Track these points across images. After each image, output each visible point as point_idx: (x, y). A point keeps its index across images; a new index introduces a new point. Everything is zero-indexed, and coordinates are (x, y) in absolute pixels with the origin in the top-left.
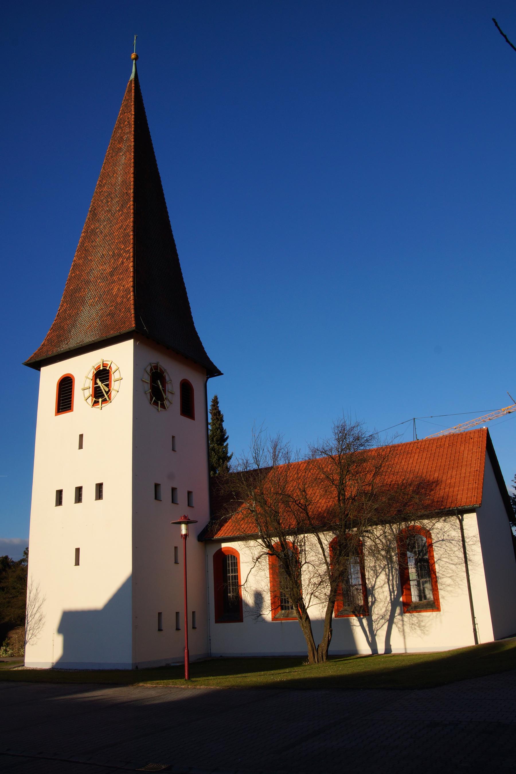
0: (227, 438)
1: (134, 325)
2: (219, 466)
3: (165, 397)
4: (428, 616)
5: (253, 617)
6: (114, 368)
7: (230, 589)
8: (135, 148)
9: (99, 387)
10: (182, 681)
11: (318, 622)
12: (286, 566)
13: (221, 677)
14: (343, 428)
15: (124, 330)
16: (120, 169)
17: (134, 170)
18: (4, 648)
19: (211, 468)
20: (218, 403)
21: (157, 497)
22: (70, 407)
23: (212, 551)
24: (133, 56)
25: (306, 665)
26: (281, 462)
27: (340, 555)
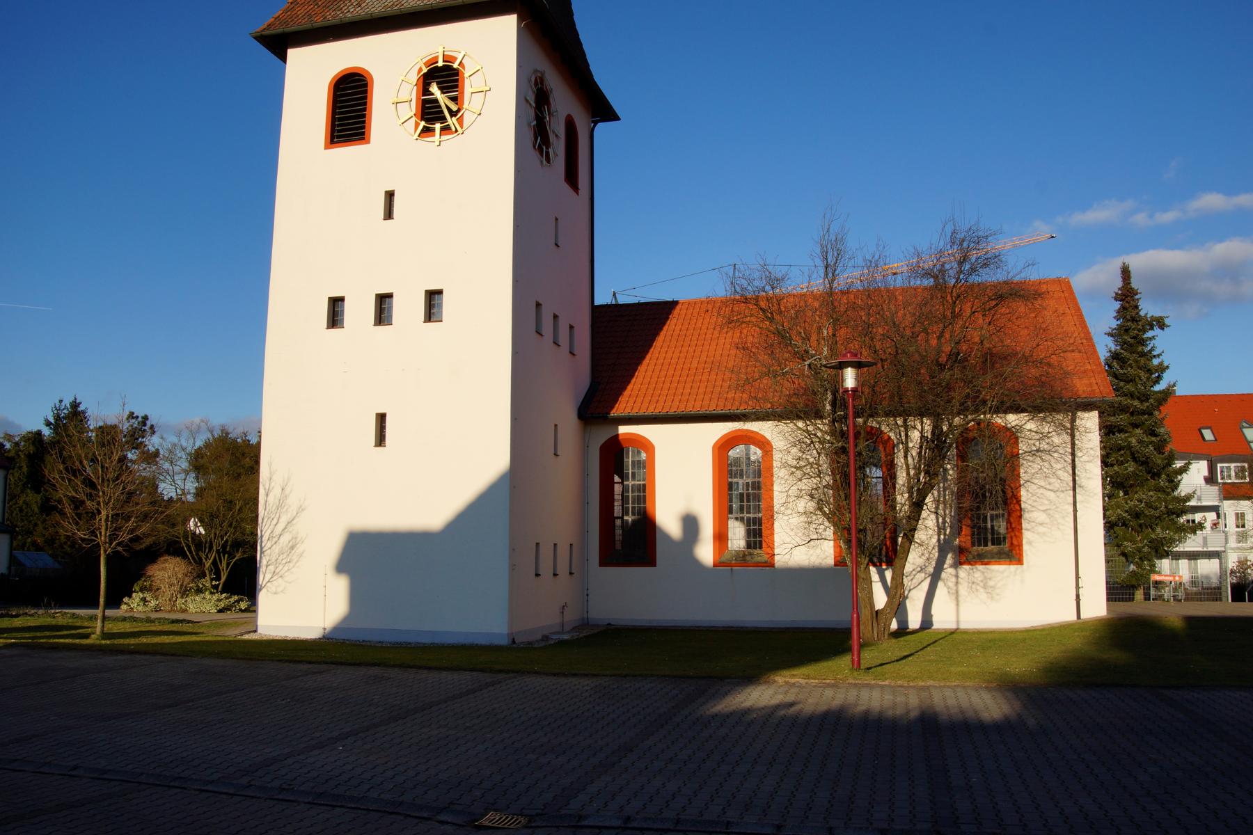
4: (1000, 572)
21: (433, 298)
22: (363, 133)
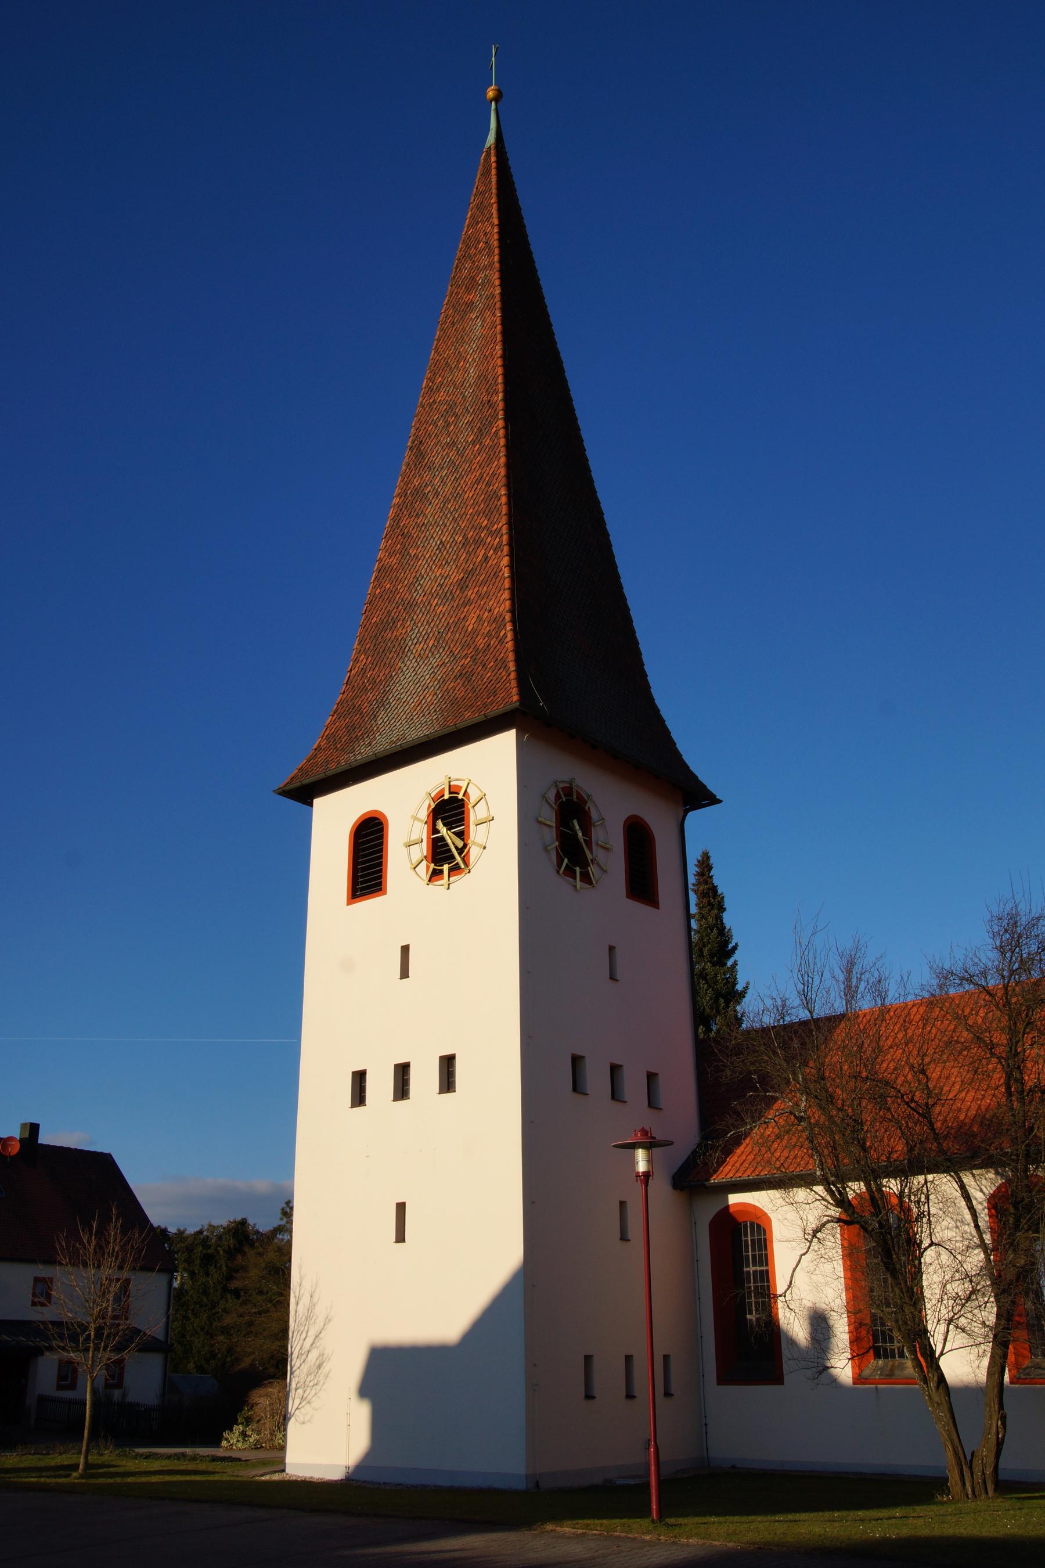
0: (735, 948)
1: (516, 698)
2: (718, 1012)
3: (589, 856)
5: (809, 1373)
6: (474, 795)
7: (750, 1303)
8: (503, 301)
9: (442, 839)
10: (645, 1523)
11: (968, 1391)
12: (883, 1251)
13: (736, 1518)
14: (1013, 920)
15: (496, 709)
16: (471, 349)
17: (504, 350)
18: (241, 1427)
19: (700, 1018)
20: (711, 868)
22: (380, 884)
23: (707, 1211)
24: (491, 94)
25: (942, 1503)
26: (865, 1004)
27: (1017, 1227)
